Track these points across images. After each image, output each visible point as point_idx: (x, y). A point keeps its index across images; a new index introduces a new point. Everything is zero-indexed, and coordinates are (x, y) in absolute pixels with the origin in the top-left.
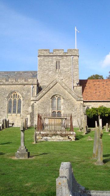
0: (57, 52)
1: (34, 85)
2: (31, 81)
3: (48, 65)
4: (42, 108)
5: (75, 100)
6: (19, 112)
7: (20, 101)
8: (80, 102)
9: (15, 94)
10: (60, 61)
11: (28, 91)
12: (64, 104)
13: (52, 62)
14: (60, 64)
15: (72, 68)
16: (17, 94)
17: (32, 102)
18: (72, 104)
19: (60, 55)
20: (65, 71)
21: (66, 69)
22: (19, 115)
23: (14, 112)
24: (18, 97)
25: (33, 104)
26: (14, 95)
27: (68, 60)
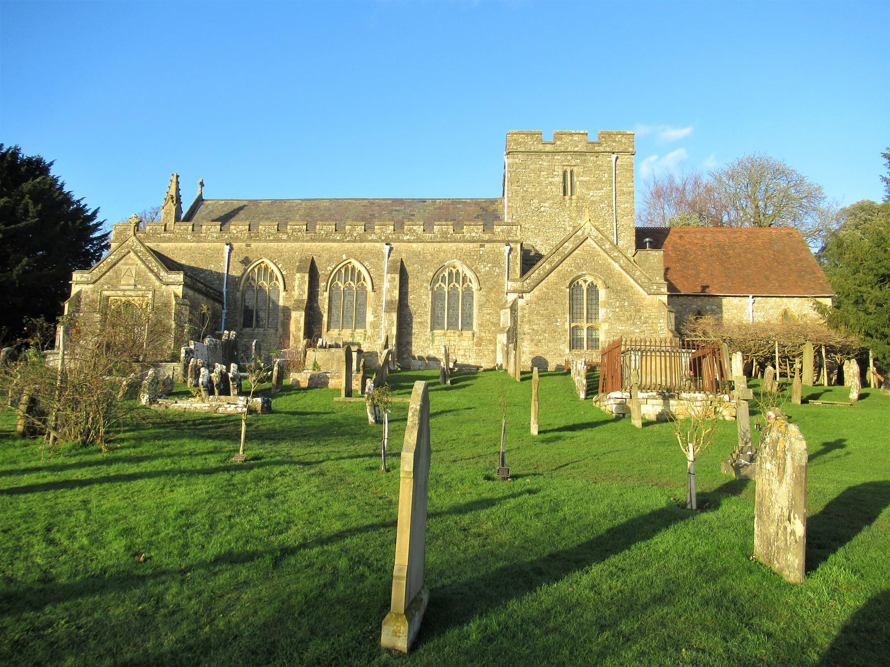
0: (567, 139)
1: (512, 245)
2: (502, 231)
3: (540, 183)
4: (542, 315)
5: (643, 293)
6: (467, 324)
7: (468, 293)
8: (659, 297)
9: (454, 271)
10: (575, 169)
11: (496, 263)
12: (608, 304)
13: (551, 172)
14: (575, 179)
15: (614, 193)
16: (460, 271)
17: (511, 297)
18: (635, 306)
19: (576, 149)
20: (593, 201)
21: (595, 195)
22: (467, 334)
23: (452, 325)
24: (359, 279)
25: (515, 302)
26: (450, 274)
27: (598, 167)
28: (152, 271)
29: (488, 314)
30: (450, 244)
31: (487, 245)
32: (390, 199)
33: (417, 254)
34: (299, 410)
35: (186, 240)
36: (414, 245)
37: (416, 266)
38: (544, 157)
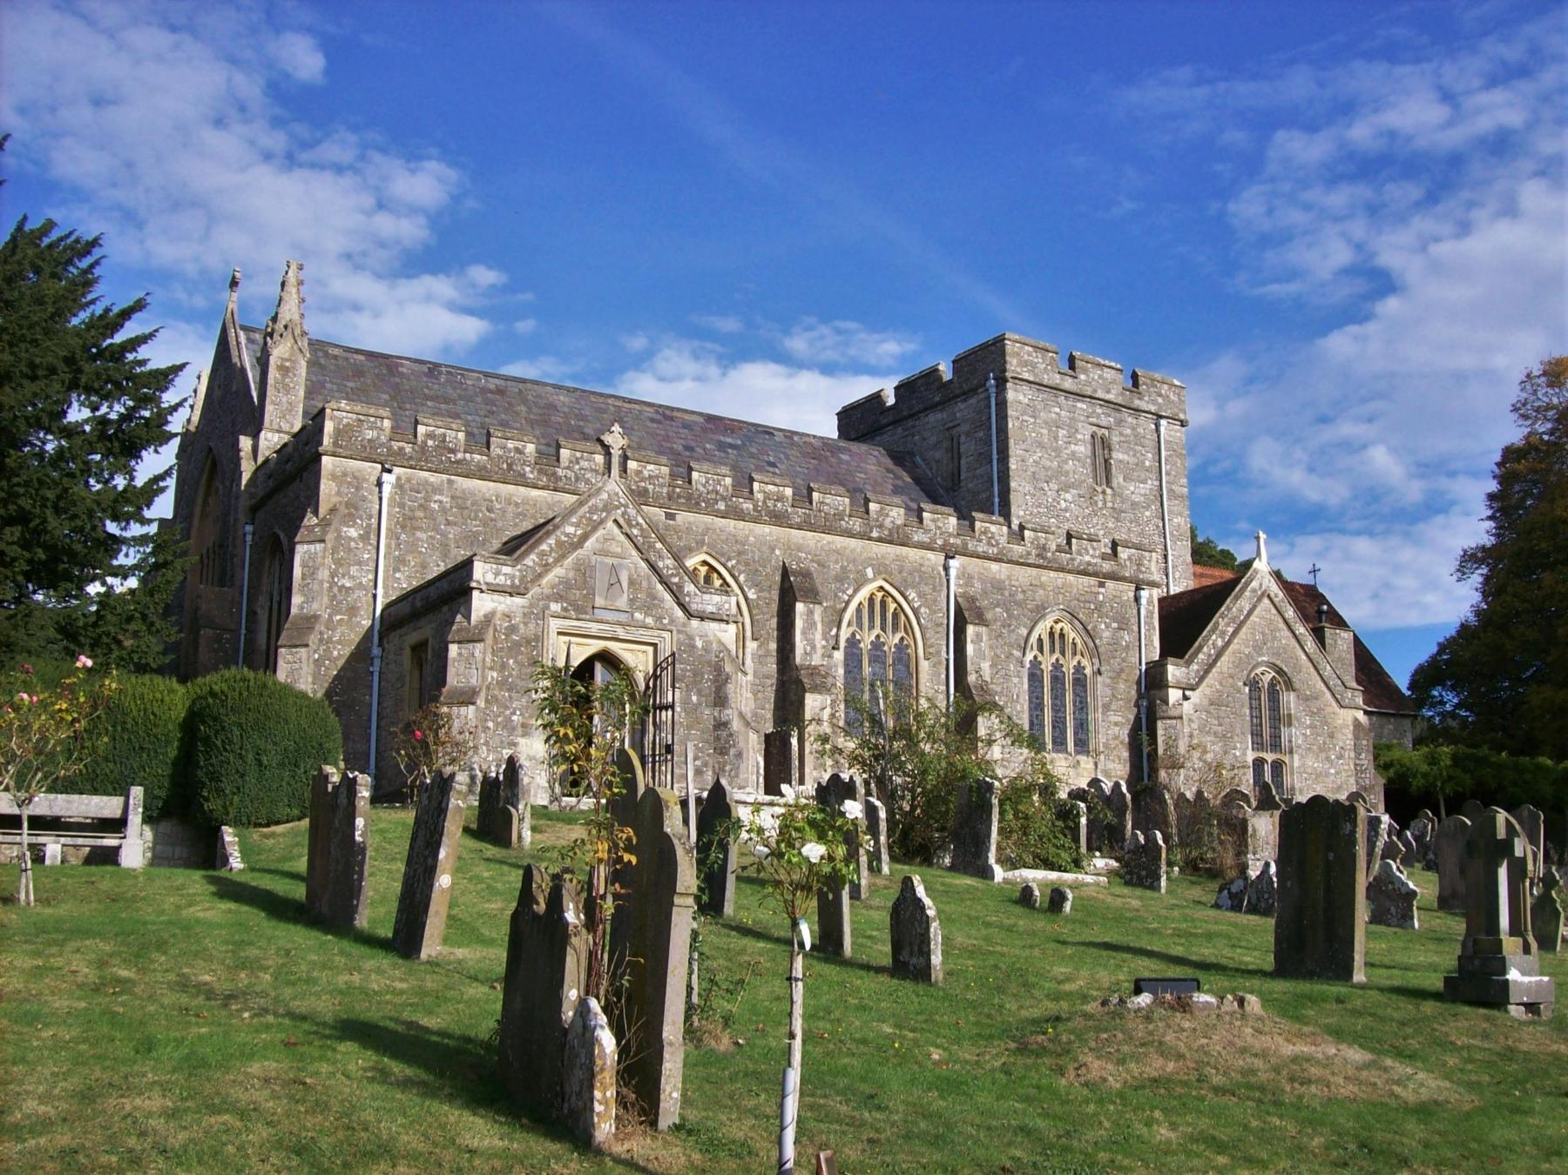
28: (664, 582)
29: (1116, 724)
30: (1052, 574)
31: (1110, 584)
32: (701, 414)
33: (998, 586)
34: (269, 876)
35: (521, 481)
36: (994, 566)
37: (998, 610)
38: (1062, 399)
